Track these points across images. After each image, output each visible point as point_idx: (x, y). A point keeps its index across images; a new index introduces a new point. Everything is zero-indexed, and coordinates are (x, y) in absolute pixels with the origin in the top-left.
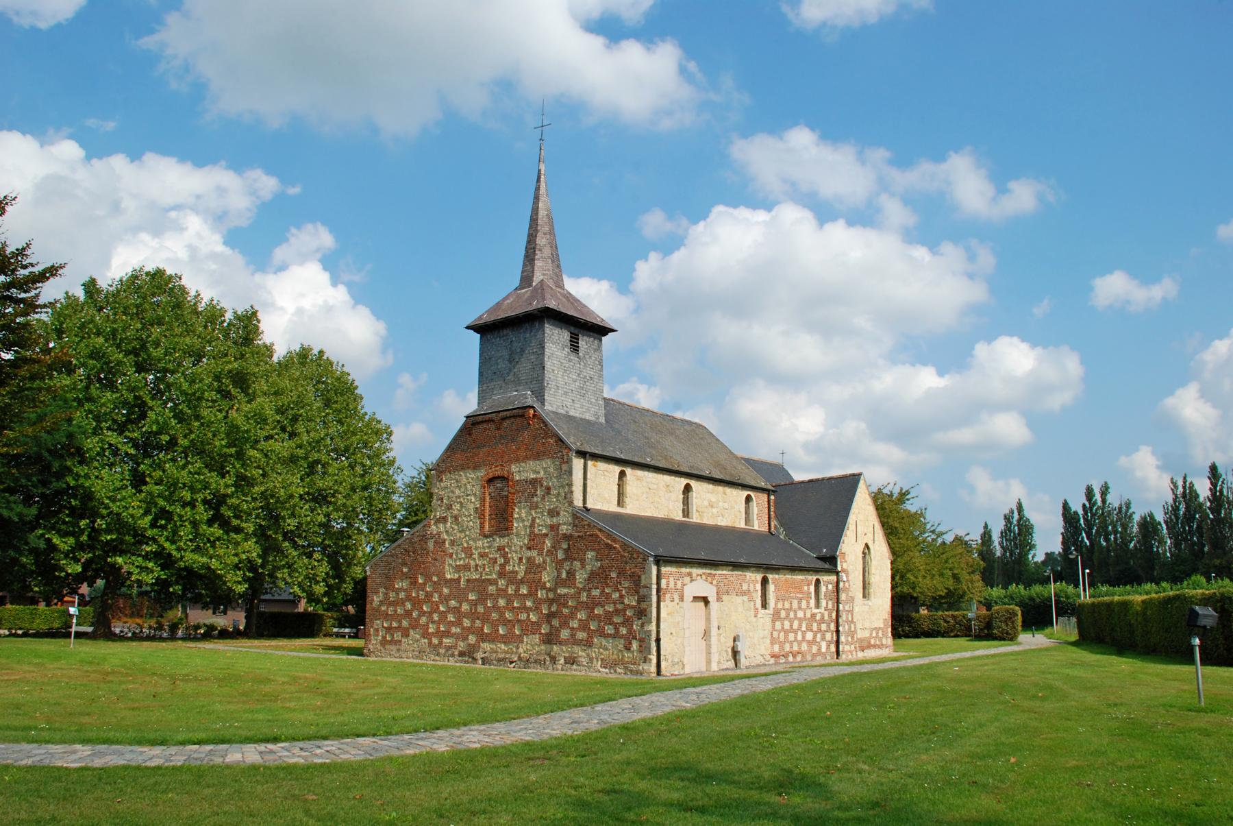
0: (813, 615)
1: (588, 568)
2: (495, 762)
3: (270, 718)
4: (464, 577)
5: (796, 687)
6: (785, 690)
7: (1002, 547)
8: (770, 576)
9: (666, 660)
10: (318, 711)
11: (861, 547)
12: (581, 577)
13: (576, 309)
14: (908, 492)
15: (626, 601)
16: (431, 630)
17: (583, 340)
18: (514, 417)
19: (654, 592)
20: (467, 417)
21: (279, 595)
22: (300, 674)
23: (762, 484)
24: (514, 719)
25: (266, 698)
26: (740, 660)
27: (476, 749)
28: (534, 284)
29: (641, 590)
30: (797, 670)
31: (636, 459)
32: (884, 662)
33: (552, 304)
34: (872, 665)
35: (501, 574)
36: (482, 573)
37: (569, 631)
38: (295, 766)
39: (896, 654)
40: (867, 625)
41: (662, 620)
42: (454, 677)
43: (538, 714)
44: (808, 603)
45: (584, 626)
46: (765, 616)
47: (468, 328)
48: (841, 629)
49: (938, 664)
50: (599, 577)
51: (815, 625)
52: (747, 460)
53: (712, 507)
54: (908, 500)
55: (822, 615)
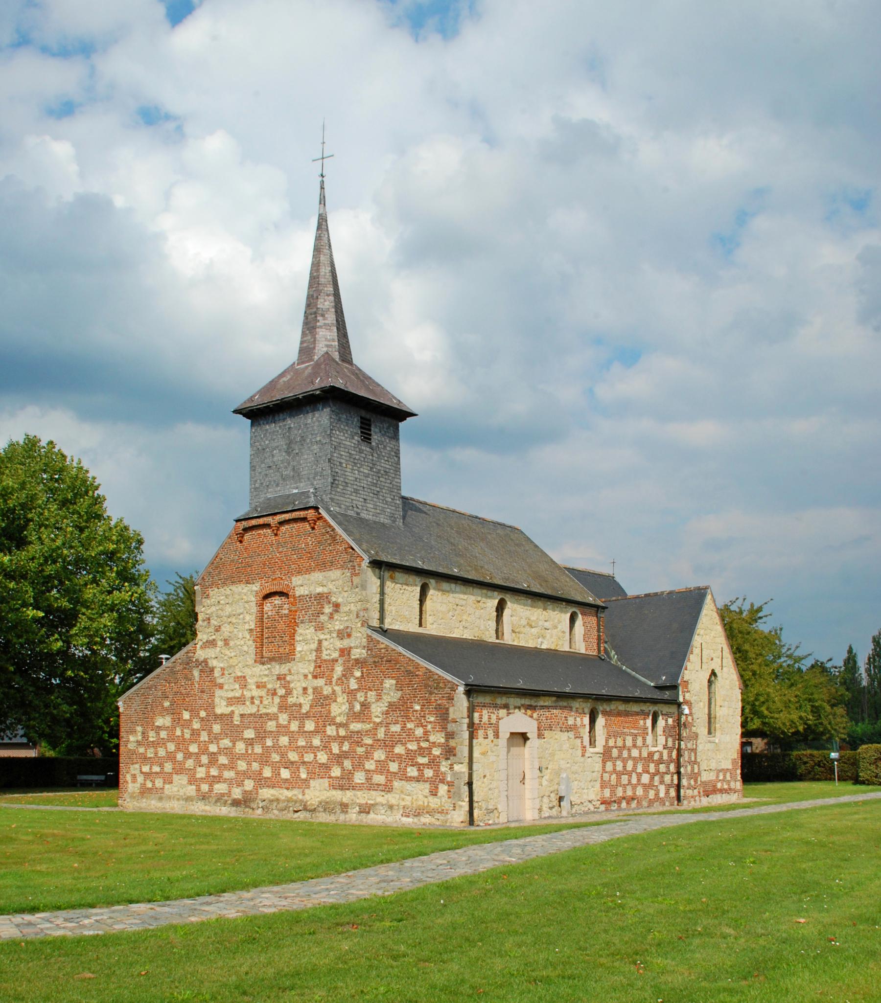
0: (651, 755)
1: (386, 699)
2: (297, 929)
3: (19, 884)
4: (239, 710)
5: (635, 838)
6: (624, 842)
7: (869, 675)
10: (76, 874)
12: (377, 710)
13: (367, 388)
14: (760, 609)
15: (432, 738)
16: (198, 776)
17: (376, 427)
18: (295, 520)
21: (10, 739)
22: (46, 831)
23: (590, 600)
24: (312, 878)
25: (10, 861)
27: (274, 913)
28: (316, 358)
29: (449, 726)
30: (633, 818)
31: (441, 570)
32: (734, 809)
33: (340, 383)
34: (721, 813)
35: (283, 707)
36: (259, 707)
37: (363, 773)
38: (64, 939)
39: (746, 800)
40: (713, 765)
41: (475, 760)
42: (230, 830)
43: (339, 873)
44: (644, 739)
45: (382, 767)
47: (236, 412)
48: (682, 770)
49: (799, 812)
51: (652, 766)
52: (572, 571)
53: (531, 627)
54: (760, 618)
55: (661, 754)
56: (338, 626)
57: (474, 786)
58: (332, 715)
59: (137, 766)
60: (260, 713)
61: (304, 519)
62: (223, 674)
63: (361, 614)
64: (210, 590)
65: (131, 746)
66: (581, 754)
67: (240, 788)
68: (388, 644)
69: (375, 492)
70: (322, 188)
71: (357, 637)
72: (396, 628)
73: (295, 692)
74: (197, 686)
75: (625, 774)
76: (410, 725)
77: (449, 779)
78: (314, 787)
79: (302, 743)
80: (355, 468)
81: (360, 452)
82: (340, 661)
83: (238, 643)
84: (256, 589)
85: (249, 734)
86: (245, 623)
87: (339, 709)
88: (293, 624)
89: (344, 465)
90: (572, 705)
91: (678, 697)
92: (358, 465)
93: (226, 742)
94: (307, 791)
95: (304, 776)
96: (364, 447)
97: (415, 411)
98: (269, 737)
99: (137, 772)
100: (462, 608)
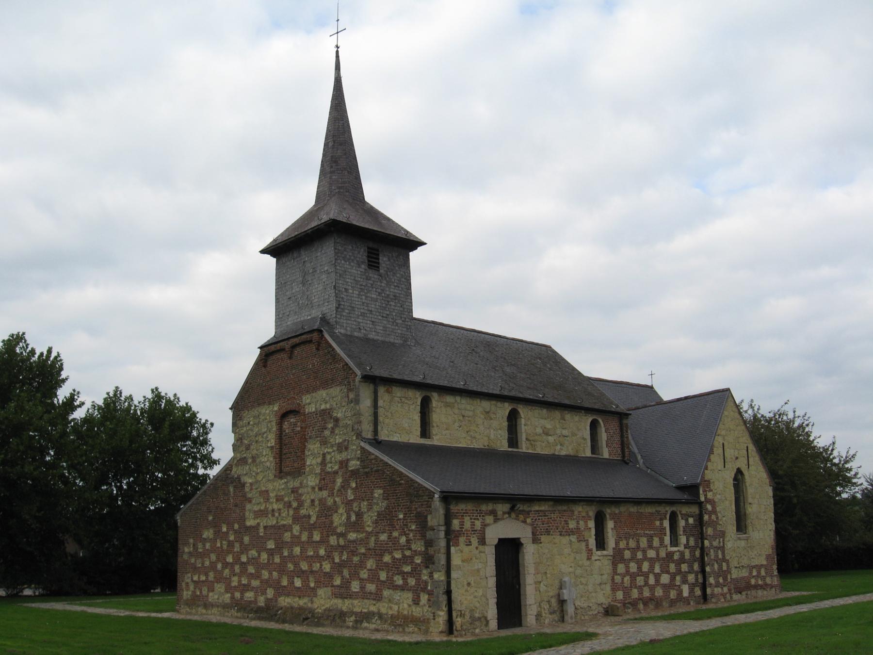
0: (670, 555)
1: (376, 508)
11: (729, 476)
15: (413, 547)
20: (261, 348)
26: (567, 611)
35: (297, 519)
36: (277, 518)
40: (745, 561)
44: (662, 541)
45: (374, 577)
46: (602, 561)
47: (263, 252)
48: (708, 569)
50: (386, 518)
53: (547, 434)
56: (339, 440)
58: (334, 525)
59: (189, 575)
60: (279, 524)
61: (310, 341)
62: (251, 489)
63: (356, 427)
64: (242, 412)
65: (185, 557)
66: (586, 558)
67: (264, 596)
68: (378, 455)
69: (385, 315)
70: (337, 56)
71: (353, 450)
72: (395, 439)
74: (232, 501)
75: (641, 576)
76: (395, 534)
80: (362, 293)
81: (367, 279)
82: (340, 473)
83: (263, 460)
85: (271, 545)
87: (339, 519)
89: (351, 291)
90: (574, 509)
91: (699, 497)
92: (366, 291)
93: (253, 553)
94: (315, 599)
95: (312, 585)
96: (372, 274)
98: (286, 548)
99: (189, 580)
100: (470, 419)
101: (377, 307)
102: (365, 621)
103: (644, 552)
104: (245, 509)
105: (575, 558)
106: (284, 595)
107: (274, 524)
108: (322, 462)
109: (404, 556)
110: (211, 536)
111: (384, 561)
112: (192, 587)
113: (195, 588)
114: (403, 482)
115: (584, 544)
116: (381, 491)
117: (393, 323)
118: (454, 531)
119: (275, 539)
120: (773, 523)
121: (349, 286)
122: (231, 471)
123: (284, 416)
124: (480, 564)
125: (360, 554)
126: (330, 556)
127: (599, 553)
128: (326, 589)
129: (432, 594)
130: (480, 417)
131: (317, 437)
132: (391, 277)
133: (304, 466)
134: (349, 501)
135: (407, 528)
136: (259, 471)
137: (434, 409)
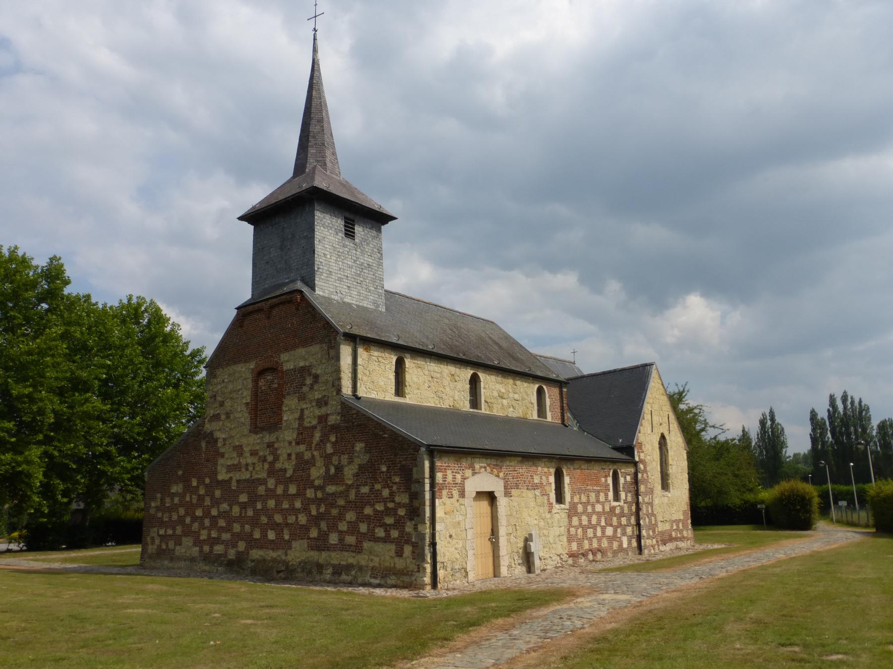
0: (613, 509)
1: (357, 461)
4: (237, 476)
8: (482, 375)
9: (445, 568)
11: (656, 439)
12: (349, 472)
15: (397, 499)
19: (427, 487)
35: (271, 472)
36: (251, 472)
39: (699, 548)
40: (667, 517)
44: (606, 495)
45: (353, 529)
47: (241, 218)
48: (641, 522)
50: (368, 471)
51: (615, 519)
53: (502, 398)
56: (317, 395)
57: (438, 547)
58: (311, 478)
59: (155, 529)
62: (224, 444)
66: (547, 512)
67: (235, 549)
69: (359, 282)
71: (333, 405)
73: (281, 458)
76: (378, 486)
77: (413, 540)
78: (295, 548)
79: (286, 505)
80: (339, 259)
81: (344, 247)
82: (319, 428)
83: (237, 416)
84: (252, 367)
86: (243, 397)
87: (316, 473)
88: (280, 397)
89: (328, 256)
93: (225, 506)
96: (348, 242)
97: (394, 215)
98: (259, 501)
99: (155, 535)
100: (438, 380)
101: (352, 273)
102: (343, 573)
103: (593, 506)
104: (217, 464)
105: (539, 511)
106: (256, 547)
107: (247, 477)
108: (300, 417)
109: (387, 509)
110: (180, 491)
111: (366, 513)
112: (157, 542)
113: (161, 542)
114: (386, 436)
115: (546, 497)
116: (363, 445)
117: (366, 289)
118: (438, 484)
119: (248, 493)
120: (687, 483)
121: (327, 251)
122: (203, 427)
123: (260, 373)
124: (460, 516)
125: (339, 506)
126: (307, 509)
127: (557, 506)
128: (301, 541)
129: (417, 546)
130: (446, 379)
131: (295, 393)
132: (365, 246)
133: (281, 421)
134: (328, 455)
135: (391, 480)
136: (233, 426)
137: (406, 369)
